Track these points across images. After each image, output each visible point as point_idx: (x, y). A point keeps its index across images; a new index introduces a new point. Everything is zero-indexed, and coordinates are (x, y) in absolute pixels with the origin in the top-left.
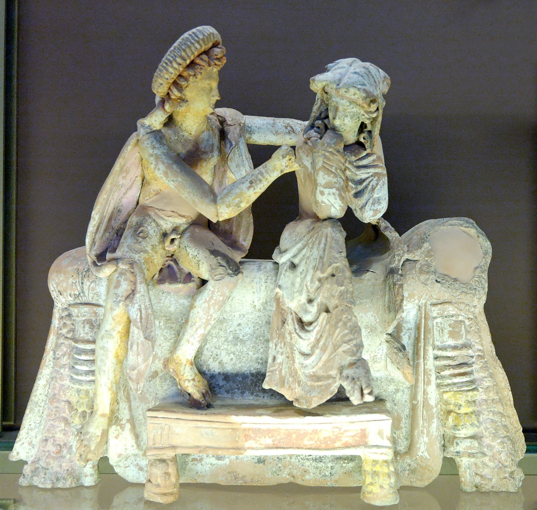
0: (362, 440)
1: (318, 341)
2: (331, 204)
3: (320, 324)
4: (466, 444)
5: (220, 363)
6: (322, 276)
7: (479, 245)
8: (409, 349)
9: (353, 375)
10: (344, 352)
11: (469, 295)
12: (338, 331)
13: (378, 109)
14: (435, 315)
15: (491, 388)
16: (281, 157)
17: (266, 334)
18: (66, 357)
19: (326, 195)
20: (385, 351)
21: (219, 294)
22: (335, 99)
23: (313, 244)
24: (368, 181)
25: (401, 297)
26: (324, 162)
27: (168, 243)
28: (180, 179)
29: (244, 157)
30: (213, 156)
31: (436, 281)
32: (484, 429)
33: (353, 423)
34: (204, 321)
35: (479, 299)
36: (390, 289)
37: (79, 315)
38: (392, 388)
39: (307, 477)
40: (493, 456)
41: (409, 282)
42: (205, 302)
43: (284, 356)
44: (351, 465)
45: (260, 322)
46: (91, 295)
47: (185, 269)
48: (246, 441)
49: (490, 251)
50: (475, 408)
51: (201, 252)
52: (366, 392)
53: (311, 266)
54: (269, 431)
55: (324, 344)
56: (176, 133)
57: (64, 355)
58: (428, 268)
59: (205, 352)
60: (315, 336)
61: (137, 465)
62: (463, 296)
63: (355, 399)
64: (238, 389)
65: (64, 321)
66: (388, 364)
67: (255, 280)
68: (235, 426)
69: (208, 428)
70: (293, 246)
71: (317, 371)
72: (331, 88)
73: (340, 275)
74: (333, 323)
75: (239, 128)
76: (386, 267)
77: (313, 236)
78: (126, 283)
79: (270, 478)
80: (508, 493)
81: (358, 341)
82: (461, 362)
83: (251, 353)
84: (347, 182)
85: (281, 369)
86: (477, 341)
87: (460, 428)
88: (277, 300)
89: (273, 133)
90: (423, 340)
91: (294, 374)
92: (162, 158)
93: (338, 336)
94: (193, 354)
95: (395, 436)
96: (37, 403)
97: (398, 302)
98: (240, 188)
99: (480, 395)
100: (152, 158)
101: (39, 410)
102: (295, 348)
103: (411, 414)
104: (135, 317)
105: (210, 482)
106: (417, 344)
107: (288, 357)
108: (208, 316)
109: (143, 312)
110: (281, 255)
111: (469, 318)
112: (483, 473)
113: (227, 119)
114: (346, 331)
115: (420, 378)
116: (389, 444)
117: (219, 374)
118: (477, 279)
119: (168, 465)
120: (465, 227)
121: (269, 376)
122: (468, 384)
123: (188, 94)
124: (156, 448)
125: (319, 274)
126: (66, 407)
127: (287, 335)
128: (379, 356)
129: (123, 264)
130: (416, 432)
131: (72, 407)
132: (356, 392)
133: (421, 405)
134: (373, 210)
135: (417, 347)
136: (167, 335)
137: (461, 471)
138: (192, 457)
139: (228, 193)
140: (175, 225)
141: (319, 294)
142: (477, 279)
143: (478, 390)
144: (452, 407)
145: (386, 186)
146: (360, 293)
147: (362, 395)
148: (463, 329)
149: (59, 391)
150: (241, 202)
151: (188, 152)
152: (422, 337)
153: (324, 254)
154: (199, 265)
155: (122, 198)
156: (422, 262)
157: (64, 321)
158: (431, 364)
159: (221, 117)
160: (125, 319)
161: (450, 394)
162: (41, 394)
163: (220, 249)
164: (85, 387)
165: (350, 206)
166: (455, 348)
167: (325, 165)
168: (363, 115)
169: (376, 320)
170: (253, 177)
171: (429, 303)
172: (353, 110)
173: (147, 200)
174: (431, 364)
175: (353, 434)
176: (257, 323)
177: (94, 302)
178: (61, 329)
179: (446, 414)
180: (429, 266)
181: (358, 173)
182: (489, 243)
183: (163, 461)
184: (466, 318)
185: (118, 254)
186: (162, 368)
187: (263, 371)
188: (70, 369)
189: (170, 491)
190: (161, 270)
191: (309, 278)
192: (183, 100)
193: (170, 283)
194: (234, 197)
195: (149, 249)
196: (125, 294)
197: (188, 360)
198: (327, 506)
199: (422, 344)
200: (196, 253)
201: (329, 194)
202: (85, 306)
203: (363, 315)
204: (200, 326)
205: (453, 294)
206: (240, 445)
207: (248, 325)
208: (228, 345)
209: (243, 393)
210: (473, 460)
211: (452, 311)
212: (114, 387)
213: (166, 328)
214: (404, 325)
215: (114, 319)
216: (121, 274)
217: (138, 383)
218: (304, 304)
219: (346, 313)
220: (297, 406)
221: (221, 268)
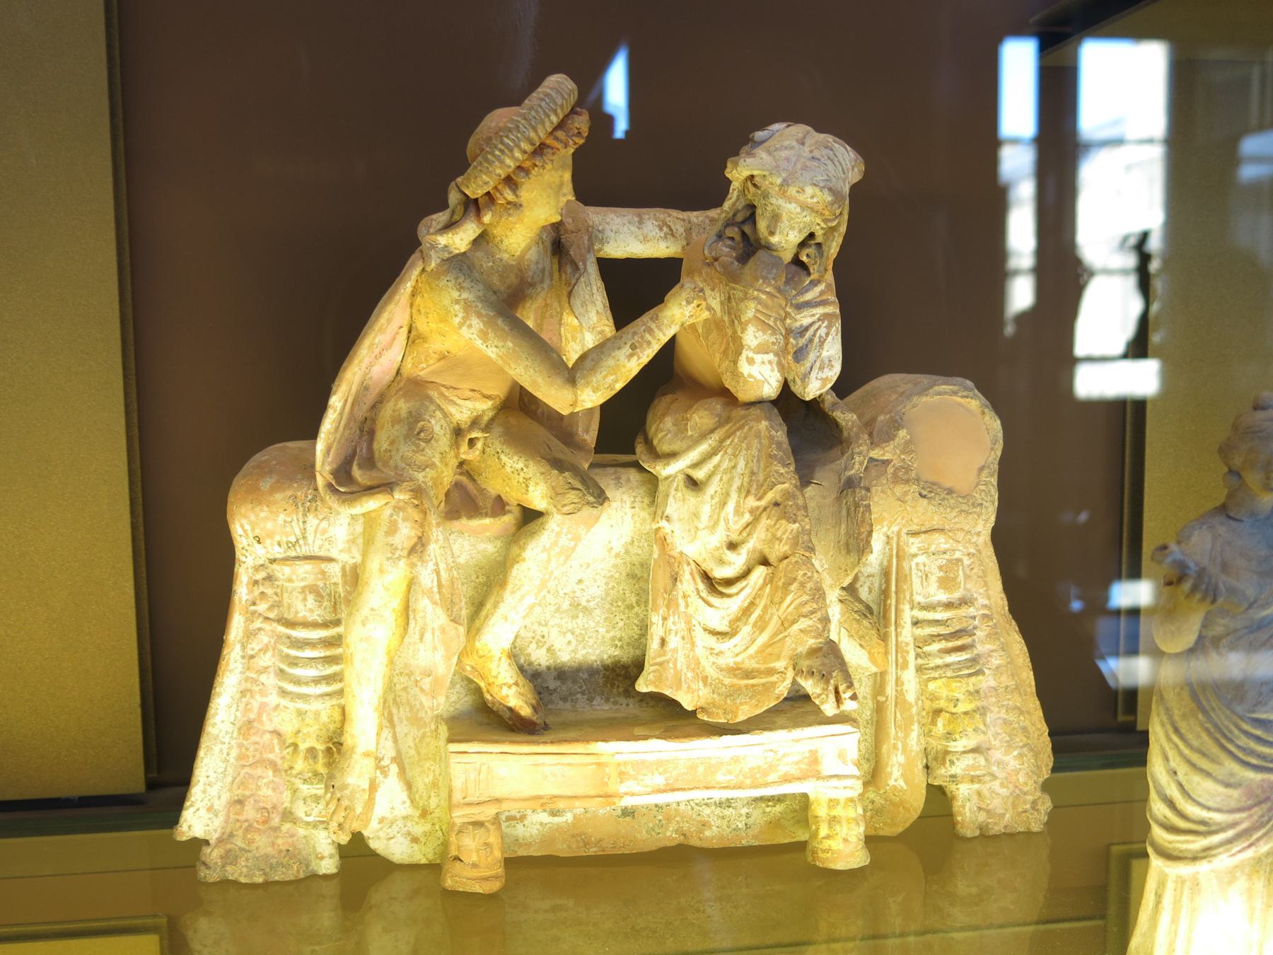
0: (812, 769)
1: (747, 611)
5: (548, 650)
6: (758, 503)
10: (801, 630)
14: (913, 550)
16: (684, 303)
18: (269, 654)
19: (756, 365)
21: (569, 536)
22: (777, 201)
23: (735, 449)
25: (868, 528)
26: (757, 310)
29: (595, 288)
33: (798, 741)
35: (986, 521)
39: (708, 833)
44: (779, 808)
45: (617, 576)
46: (318, 542)
47: (490, 489)
50: (979, 704)
51: (531, 463)
52: (846, 695)
54: (660, 763)
55: (760, 617)
57: (264, 650)
61: (409, 833)
62: (962, 518)
64: (583, 693)
65: (262, 589)
68: (603, 759)
70: (689, 448)
74: (780, 584)
78: (408, 524)
79: (645, 837)
80: (1029, 834)
82: (958, 628)
83: (602, 630)
91: (695, 665)
99: (986, 682)
100: (457, 307)
102: (694, 622)
106: (885, 601)
107: (683, 638)
109: (444, 574)
114: (805, 598)
117: (548, 668)
118: (983, 487)
119: (488, 831)
123: (526, 194)
125: (752, 502)
126: (275, 741)
130: (884, 748)
135: (885, 605)
137: (957, 805)
138: (507, 814)
141: (749, 534)
142: (983, 487)
143: (983, 673)
144: (942, 704)
148: (961, 573)
149: (260, 714)
150: (616, 381)
151: (509, 287)
152: (893, 588)
156: (896, 463)
157: (262, 589)
161: (939, 682)
164: (316, 705)
166: (949, 605)
171: (905, 531)
174: (907, 633)
176: (612, 577)
177: (322, 554)
178: (254, 604)
180: (908, 469)
182: (999, 422)
183: (479, 824)
188: (276, 674)
192: (517, 206)
193: (470, 517)
195: (436, 460)
199: (893, 601)
209: (590, 700)
210: (976, 786)
215: (387, 589)
216: (397, 508)
220: (706, 718)
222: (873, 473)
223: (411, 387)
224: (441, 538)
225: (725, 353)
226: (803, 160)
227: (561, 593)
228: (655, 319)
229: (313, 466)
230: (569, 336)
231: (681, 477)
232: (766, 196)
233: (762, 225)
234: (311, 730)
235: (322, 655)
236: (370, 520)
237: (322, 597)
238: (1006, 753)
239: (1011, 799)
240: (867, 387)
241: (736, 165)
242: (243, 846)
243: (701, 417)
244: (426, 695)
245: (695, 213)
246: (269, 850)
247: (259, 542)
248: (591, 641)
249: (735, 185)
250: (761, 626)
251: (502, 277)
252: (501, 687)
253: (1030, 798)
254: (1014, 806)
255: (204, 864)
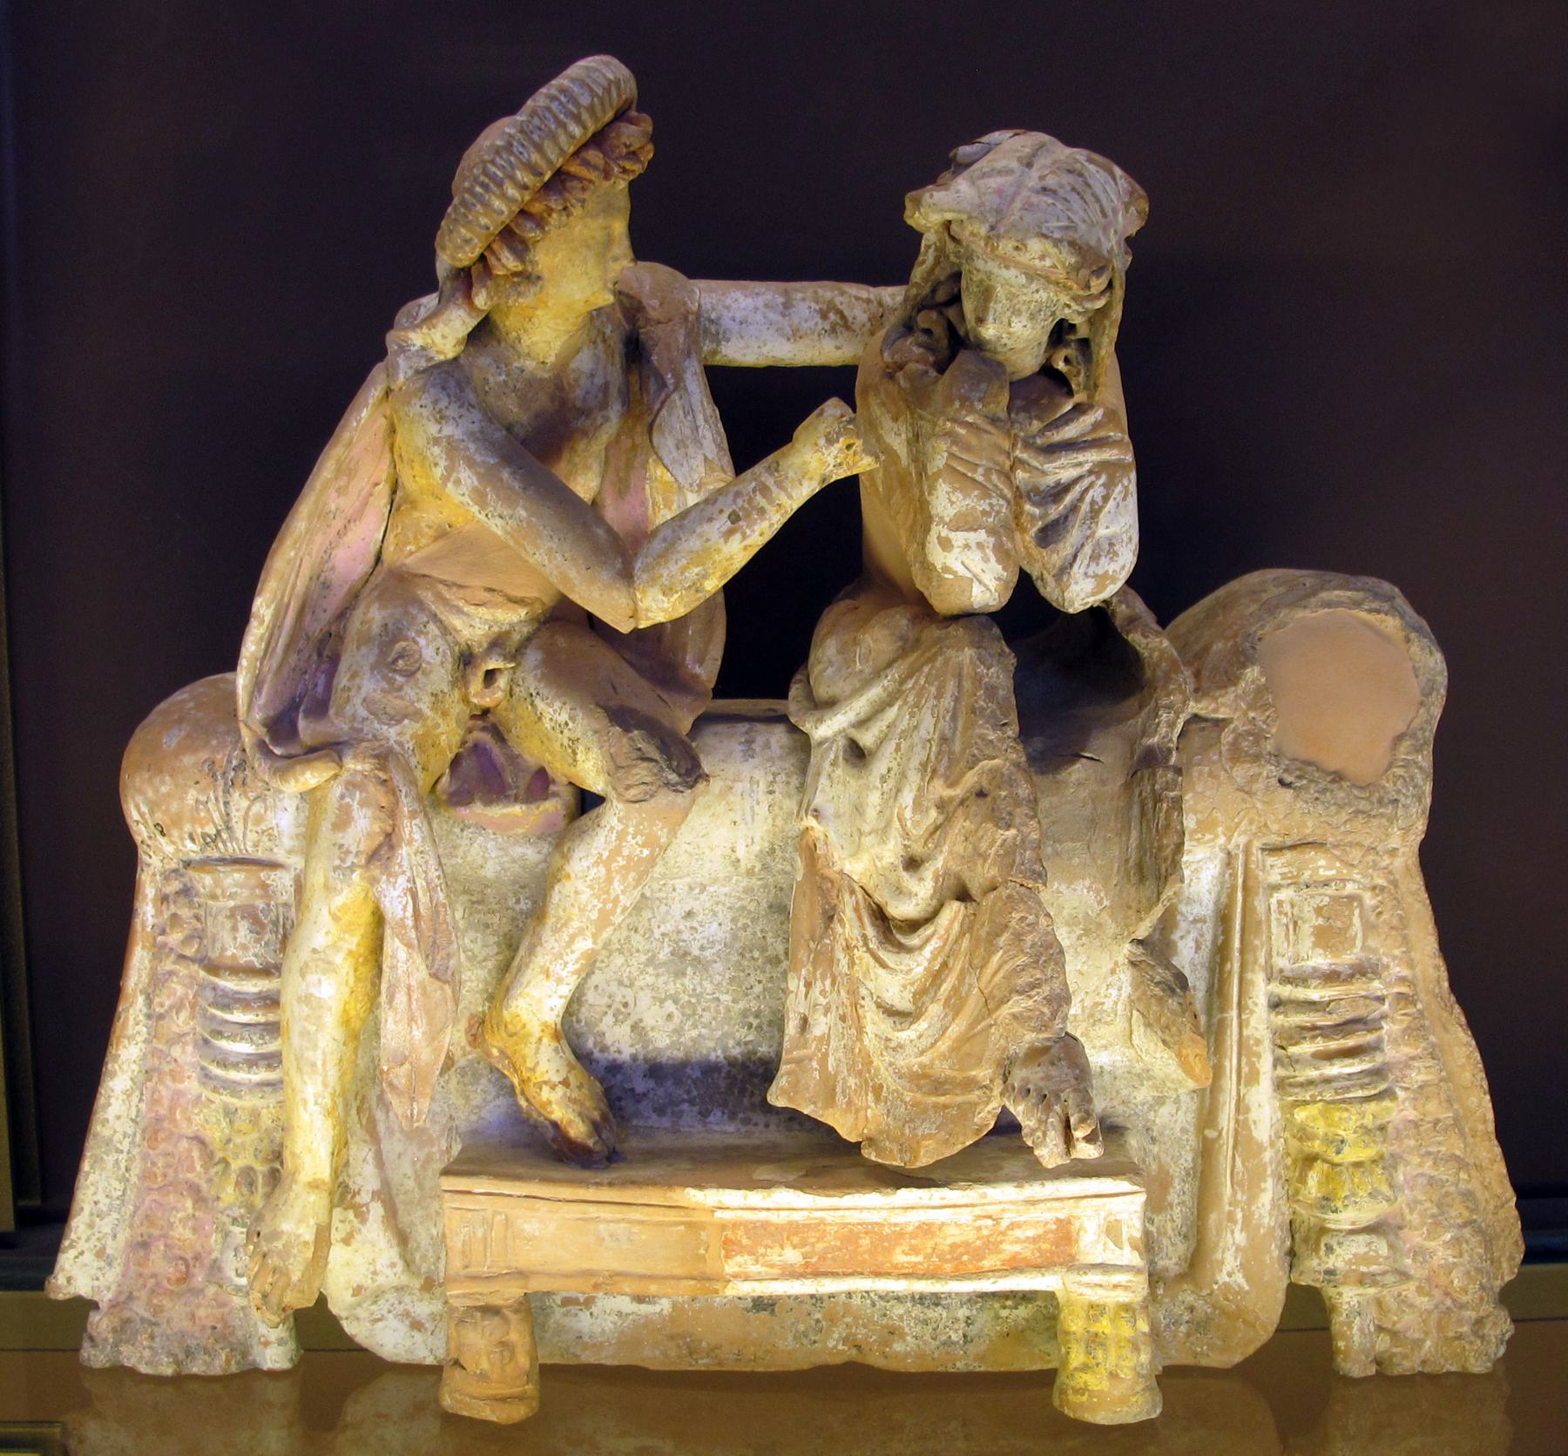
1: (936, 977)
2: (971, 571)
3: (942, 931)
4: (1354, 1250)
5: (634, 1027)
6: (948, 793)
7: (1410, 665)
8: (1198, 982)
9: (1041, 1084)
10: (1014, 1016)
11: (1375, 822)
12: (996, 959)
13: (1110, 285)
14: (1274, 877)
15: (1432, 1089)
16: (822, 442)
17: (770, 940)
18: (184, 1014)
19: (956, 551)
20: (1127, 990)
21: (640, 839)
22: (984, 265)
23: (919, 695)
24: (1078, 489)
27: (476, 684)
28: (523, 513)
29: (700, 419)
30: (607, 419)
31: (1281, 782)
32: (1408, 1205)
34: (594, 916)
35: (1406, 830)
36: (1143, 813)
37: (219, 892)
38: (1144, 1094)
39: (898, 1347)
40: (1428, 1280)
41: (1199, 788)
42: (597, 864)
43: (832, 1016)
44: (1023, 1312)
45: (752, 907)
46: (252, 836)
47: (527, 757)
48: (727, 1257)
49: (1442, 680)
50: (1385, 1149)
51: (580, 714)
53: (915, 762)
54: (793, 1229)
55: (955, 990)
56: (501, 362)
57: (178, 1007)
58: (1257, 742)
59: (590, 996)
60: (926, 964)
61: (407, 1314)
63: (1049, 1153)
64: (692, 1102)
65: (173, 909)
66: (1134, 1027)
67: (739, 787)
68: (696, 1217)
69: (618, 1221)
70: (856, 692)
71: (932, 1063)
72: (972, 234)
73: (1003, 793)
74: (983, 933)
75: (682, 331)
76: (1132, 744)
77: (919, 669)
78: (368, 812)
79: (790, 1350)
80: (1465, 1377)
81: (1056, 985)
82: (1348, 1016)
84: (1017, 504)
85: (826, 1055)
86: (1397, 952)
87: (1339, 1204)
88: (810, 851)
89: (783, 335)
90: (1237, 954)
91: (862, 1064)
92: (467, 449)
93: (996, 972)
94: (559, 1004)
95: (1153, 1229)
96: (109, 1142)
97: (1168, 851)
98: (700, 536)
99: (1398, 1111)
100: (436, 450)
101: (117, 1162)
102: (864, 992)
103: (1199, 1168)
104: (400, 914)
105: (616, 1363)
107: (843, 1018)
108: (605, 902)
109: (423, 899)
110: (817, 714)
111: (1374, 888)
112: (1399, 1327)
113: (645, 302)
115: (1227, 1063)
116: (1131, 1257)
118: (1400, 772)
119: (506, 1321)
120: (1370, 611)
121: (789, 1073)
122: (1367, 1080)
123: (544, 258)
124: (473, 1278)
125: (939, 789)
126: (196, 1154)
127: (840, 955)
128: (1108, 1005)
129: (355, 757)
130: (1213, 1218)
131: (211, 1155)
132: (1052, 1133)
133: (1228, 1141)
134: (1095, 576)
135: (1221, 972)
136: (476, 947)
137: (1338, 1320)
138: (565, 1294)
139: (667, 549)
140: (496, 629)
142: (1400, 772)
144: (1317, 1146)
145: (1132, 502)
146: (1054, 823)
147: (1068, 1140)
148: (1356, 920)
149: (172, 1110)
150: (705, 576)
151: (537, 416)
152: (1237, 944)
153: (955, 729)
154: (575, 753)
155: (332, 546)
156: (1239, 725)
157: (173, 909)
158: (1260, 1022)
159: (628, 296)
160: (366, 916)
161: (1313, 1110)
162: (118, 1118)
163: (636, 704)
164: (248, 1102)
165: (1027, 569)
166: (1331, 977)
167: (955, 464)
168: (1069, 306)
169: (1100, 902)
170: (740, 502)
171: (1257, 844)
172: (1037, 296)
173: (411, 553)
174: (1260, 1022)
175: (1031, 1233)
176: (743, 908)
177: (260, 854)
178: (163, 932)
179: (1299, 1164)
180: (1258, 736)
181: (1048, 467)
182: (1439, 656)
183: (491, 1311)
184: (1365, 888)
185: (336, 724)
186: (464, 1042)
187: (764, 1050)
188: (196, 1045)
189: (517, 1390)
190: (455, 763)
191: (907, 797)
192: (528, 277)
193: (488, 802)
194: (684, 562)
195: (425, 706)
196: (366, 846)
197: (546, 1025)
198: (953, 1425)
200: (564, 717)
201: (967, 546)
202: (237, 867)
203: (1063, 888)
204: (581, 931)
205: (1329, 820)
206: (710, 1268)
207: (715, 914)
208: (657, 975)
209: (704, 1114)
210: (1372, 1291)
211: (1326, 869)
212: (341, 1107)
213: (470, 926)
214: (1183, 908)
215: (335, 918)
216: (352, 786)
217: (412, 1100)
218: (893, 867)
219: (1022, 907)
221: (645, 764)
222: (1196, 740)
223: (393, 583)
224: (417, 836)
225: (912, 531)
226: (1025, 193)
227: (657, 934)
228: (774, 469)
229: (234, 714)
230: (659, 499)
231: (841, 742)
232: (970, 257)
233: (968, 306)
234: (248, 1139)
235: (261, 1019)
236: (311, 799)
237: (263, 926)
238: (1430, 1236)
239: (1435, 1315)
240: (1221, 592)
241: (918, 203)
242: (147, 1315)
243: (878, 639)
244: (400, 1094)
245: (890, 290)
246: (186, 1324)
247: (162, 833)
248: (707, 1017)
249: (929, 238)
250: (955, 1005)
251: (523, 400)
252: (539, 1086)
253: (1470, 1314)
254: (1440, 1327)
255: (92, 1339)
